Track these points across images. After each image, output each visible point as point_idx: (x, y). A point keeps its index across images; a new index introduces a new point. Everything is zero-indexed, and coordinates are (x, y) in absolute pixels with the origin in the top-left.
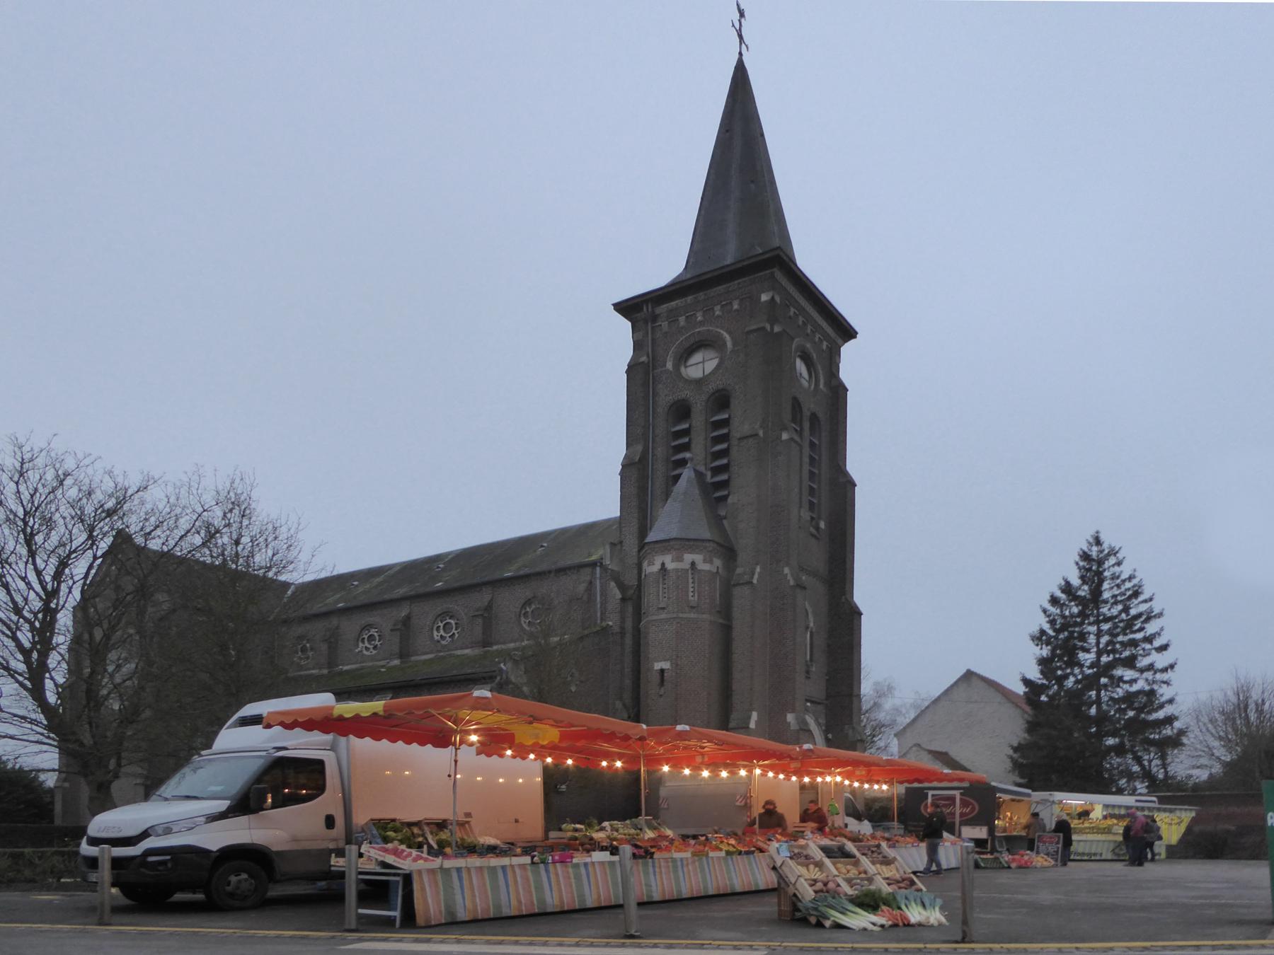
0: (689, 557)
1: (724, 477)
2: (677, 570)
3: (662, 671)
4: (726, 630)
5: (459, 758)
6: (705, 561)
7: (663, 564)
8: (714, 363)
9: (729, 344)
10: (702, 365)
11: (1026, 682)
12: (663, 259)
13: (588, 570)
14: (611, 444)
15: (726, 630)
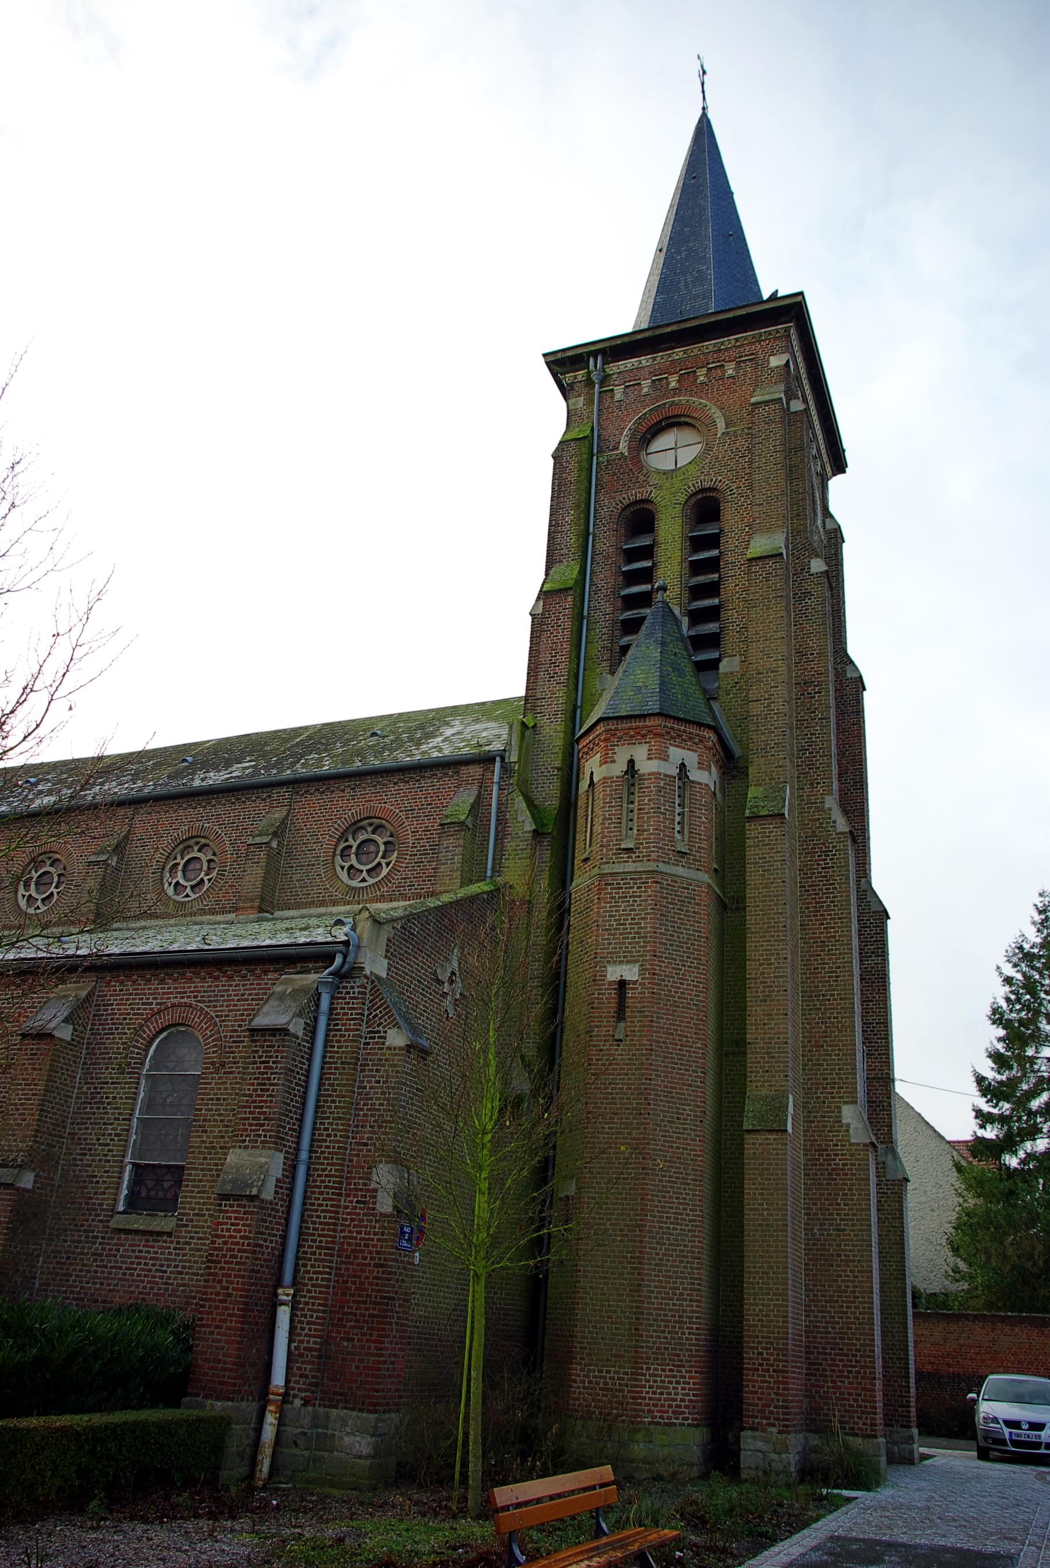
0: (677, 754)
1: (712, 627)
2: (657, 775)
3: (622, 984)
4: (731, 906)
5: (72, 668)
6: (701, 766)
7: (631, 763)
8: (695, 451)
9: (721, 425)
10: (674, 454)
11: (1000, 1039)
12: (616, 306)
13: (476, 771)
14: (520, 566)
15: (731, 906)
